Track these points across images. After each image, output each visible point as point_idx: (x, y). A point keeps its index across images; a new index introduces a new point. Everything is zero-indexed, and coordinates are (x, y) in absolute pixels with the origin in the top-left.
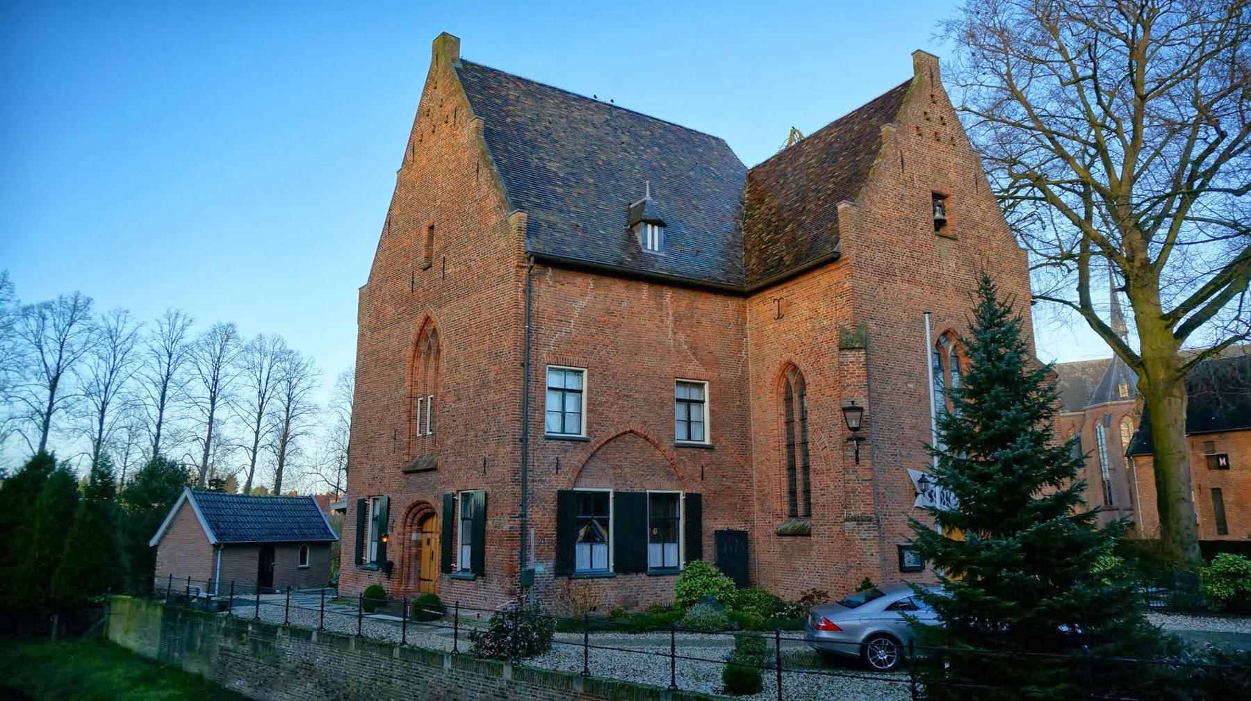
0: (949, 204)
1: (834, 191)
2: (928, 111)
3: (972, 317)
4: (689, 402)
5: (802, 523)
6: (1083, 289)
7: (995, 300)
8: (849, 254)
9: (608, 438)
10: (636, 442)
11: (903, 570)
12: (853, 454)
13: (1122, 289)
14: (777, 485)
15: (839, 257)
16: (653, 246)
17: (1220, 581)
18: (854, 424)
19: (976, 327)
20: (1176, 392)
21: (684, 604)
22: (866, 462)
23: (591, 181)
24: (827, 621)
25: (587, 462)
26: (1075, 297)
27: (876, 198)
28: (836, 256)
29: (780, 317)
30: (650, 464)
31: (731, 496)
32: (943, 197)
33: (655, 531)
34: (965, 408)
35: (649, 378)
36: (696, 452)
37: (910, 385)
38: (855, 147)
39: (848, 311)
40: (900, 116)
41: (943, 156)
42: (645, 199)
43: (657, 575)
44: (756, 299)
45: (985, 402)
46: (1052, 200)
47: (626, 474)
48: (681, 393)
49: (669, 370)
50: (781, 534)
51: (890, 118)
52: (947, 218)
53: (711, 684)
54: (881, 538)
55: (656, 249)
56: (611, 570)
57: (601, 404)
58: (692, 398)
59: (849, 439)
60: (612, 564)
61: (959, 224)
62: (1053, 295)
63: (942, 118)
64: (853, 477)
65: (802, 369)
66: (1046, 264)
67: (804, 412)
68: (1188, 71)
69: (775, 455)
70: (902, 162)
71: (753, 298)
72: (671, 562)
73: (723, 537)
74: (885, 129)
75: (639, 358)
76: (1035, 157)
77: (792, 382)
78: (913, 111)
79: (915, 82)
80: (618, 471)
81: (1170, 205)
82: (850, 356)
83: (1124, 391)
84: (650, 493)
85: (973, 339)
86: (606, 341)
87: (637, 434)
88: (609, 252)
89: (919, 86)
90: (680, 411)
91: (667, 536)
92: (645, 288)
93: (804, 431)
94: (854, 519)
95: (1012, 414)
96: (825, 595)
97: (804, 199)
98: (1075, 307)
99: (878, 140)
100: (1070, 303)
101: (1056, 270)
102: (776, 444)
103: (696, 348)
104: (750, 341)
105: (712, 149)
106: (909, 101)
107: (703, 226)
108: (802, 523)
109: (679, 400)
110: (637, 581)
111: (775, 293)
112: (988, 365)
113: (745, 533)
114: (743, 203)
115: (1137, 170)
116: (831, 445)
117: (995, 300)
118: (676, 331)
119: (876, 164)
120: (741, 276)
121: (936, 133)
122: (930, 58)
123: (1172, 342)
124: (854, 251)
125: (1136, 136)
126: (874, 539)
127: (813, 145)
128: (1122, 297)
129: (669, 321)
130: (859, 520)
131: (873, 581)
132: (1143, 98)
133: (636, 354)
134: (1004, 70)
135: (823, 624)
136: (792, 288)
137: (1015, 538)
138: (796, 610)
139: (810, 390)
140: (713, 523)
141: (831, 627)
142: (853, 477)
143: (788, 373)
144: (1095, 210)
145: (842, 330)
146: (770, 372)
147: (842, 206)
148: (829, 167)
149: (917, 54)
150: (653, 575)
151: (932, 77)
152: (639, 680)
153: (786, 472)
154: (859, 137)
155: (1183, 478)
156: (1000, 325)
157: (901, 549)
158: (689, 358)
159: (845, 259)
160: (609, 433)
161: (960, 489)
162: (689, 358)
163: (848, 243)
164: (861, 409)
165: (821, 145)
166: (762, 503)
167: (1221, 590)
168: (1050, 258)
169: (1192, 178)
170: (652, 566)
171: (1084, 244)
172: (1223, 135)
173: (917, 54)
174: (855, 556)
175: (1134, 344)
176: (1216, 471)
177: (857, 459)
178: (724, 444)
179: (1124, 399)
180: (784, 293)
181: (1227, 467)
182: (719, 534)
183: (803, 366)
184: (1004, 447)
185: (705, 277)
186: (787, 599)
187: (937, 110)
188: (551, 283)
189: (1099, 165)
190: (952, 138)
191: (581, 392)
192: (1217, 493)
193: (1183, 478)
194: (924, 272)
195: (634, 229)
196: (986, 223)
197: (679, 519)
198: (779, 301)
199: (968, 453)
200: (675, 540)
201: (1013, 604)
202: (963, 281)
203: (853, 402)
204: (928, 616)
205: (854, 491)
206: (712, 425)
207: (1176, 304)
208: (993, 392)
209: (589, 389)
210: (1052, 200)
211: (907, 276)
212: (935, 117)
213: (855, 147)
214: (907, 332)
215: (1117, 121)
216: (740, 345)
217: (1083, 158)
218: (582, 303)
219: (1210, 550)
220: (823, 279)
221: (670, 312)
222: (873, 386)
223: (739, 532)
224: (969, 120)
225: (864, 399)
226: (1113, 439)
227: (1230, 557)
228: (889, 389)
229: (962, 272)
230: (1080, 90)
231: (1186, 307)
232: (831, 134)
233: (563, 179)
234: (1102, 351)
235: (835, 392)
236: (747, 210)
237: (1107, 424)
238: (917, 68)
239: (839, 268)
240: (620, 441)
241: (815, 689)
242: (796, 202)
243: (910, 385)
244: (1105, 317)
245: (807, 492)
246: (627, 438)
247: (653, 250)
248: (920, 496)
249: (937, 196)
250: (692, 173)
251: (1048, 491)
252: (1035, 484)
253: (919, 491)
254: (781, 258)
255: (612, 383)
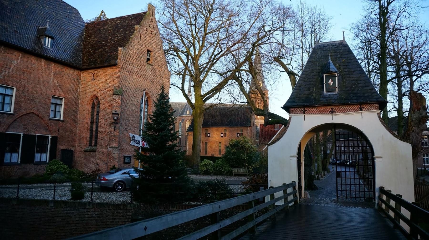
0: (152, 54)
1: (117, 42)
2: (150, 24)
3: (158, 97)
4: (56, 104)
5: (93, 148)
6: (183, 84)
7: (164, 92)
8: (120, 64)
9: (23, 114)
10: (33, 117)
11: (125, 163)
12: (114, 127)
13: (192, 86)
14: (86, 135)
15: (117, 65)
16: (48, 45)
17: (203, 166)
18: (115, 118)
19: (159, 99)
20: (201, 116)
21: (49, 174)
22: (118, 130)
23: (23, 13)
24: (104, 178)
25: (13, 122)
26: (180, 86)
27: (131, 48)
28: (116, 64)
29: (93, 80)
30: (39, 125)
31: (68, 138)
32: (151, 52)
33: (38, 149)
34: (153, 120)
35: (41, 94)
36: (56, 122)
37: (133, 108)
38: (126, 28)
39: (117, 82)
40: (142, 23)
41: (152, 39)
42: (46, 27)
43: (37, 164)
44: (85, 72)
45: (159, 120)
46: (179, 56)
47: (29, 128)
48: (53, 101)
49: (50, 92)
50: (85, 151)
51: (138, 23)
52: (150, 58)
53: (66, 198)
54: (119, 153)
55: (49, 47)
56: (19, 162)
57: (21, 102)
58: (57, 103)
59: (113, 123)
60: (19, 160)
61: (154, 61)
62: (175, 84)
63: (154, 27)
64: (112, 135)
65: (99, 98)
66: (174, 74)
67: (98, 112)
68: (218, 29)
69: (86, 125)
70: (140, 38)
71: (84, 71)
72: (44, 159)
73: (64, 151)
74: (136, 26)
75: (38, 86)
76: (177, 41)
77: (95, 102)
78: (146, 22)
79: (148, 13)
80: (25, 126)
81: (207, 65)
82: (117, 97)
83: (188, 113)
84: (38, 135)
85: (157, 102)
86: (25, 78)
87: (35, 114)
88: (28, 44)
89: (148, 15)
90: (52, 107)
91: (43, 150)
92: (43, 62)
93: (98, 118)
94: (112, 147)
95: (165, 123)
96: (100, 170)
97: (106, 41)
98: (180, 89)
99: (134, 29)
100: (179, 88)
101: (177, 76)
102: (87, 122)
103: (61, 86)
104: (81, 85)
105: (73, 12)
106: (145, 19)
107: (68, 41)
108: (93, 148)
109: (53, 103)
110: (29, 167)
111: (93, 71)
112: (160, 110)
113: (72, 151)
114: (83, 36)
115: (202, 52)
116: (106, 124)
117: (164, 92)
118: (54, 78)
119: (132, 37)
120: (80, 63)
121: (151, 31)
122: (153, 7)
123: (202, 103)
124: (122, 64)
125: (203, 44)
126: (117, 154)
127: (111, 23)
128: (192, 89)
129: (52, 75)
130: (113, 148)
131: (116, 166)
132: (206, 34)
133: (37, 85)
134: (172, 13)
135: (103, 179)
136: (99, 71)
137: (162, 155)
138: (90, 175)
139: (101, 105)
140: (62, 147)
141: (105, 180)
142: (112, 135)
143: (94, 99)
144: (189, 61)
145: (115, 88)
146: (88, 98)
147: (120, 48)
148: (116, 32)
149: (150, 4)
150: (36, 164)
151: (153, 13)
152: (39, 198)
153: (89, 131)
154: (127, 25)
155: (199, 139)
156: (165, 99)
157: (125, 157)
158: (58, 89)
159: (119, 66)
160: (23, 112)
161: (149, 142)
162: (58, 89)
163: (120, 61)
164: (118, 114)
165: (114, 24)
166: (79, 141)
167: (203, 169)
168: (176, 73)
169: (214, 59)
170: (36, 161)
171: (185, 70)
172: (222, 51)
173: (150, 4)
174: (110, 159)
175: (193, 101)
176: (207, 138)
177: (115, 129)
178: (68, 120)
179: (188, 115)
180: (96, 72)
181: (209, 137)
182: (63, 150)
183: (100, 97)
184: (162, 132)
185: (68, 61)
186: (86, 172)
187: (153, 24)
188: (3, 52)
189: (192, 48)
190: (156, 34)
191: (12, 96)
192: (206, 143)
193: (199, 139)
194: (142, 74)
195: (41, 37)
196: (161, 62)
197: (48, 145)
198: (94, 74)
199: (152, 133)
200: (46, 152)
201: (159, 171)
202: (152, 78)
203: (116, 112)
204: (136, 176)
205: (113, 139)
206: (64, 113)
207: (205, 93)
208: (161, 117)
209: (16, 95)
210: (179, 56)
211: (137, 74)
212: (152, 26)
213: (126, 28)
214: (135, 91)
215: (199, 38)
216: (78, 87)
217: (189, 45)
218: (16, 62)
219: (203, 158)
220: (110, 71)
221: (53, 71)
222: (122, 107)
223: (70, 150)
224: (160, 26)
225: (119, 111)
226: (184, 126)
227: (206, 160)
228: (127, 108)
229: (152, 76)
230: (191, 26)
231: (207, 94)
232: (118, 21)
233: (10, 10)
234: (185, 101)
235: (109, 107)
236: (85, 39)
237: (182, 122)
238: (149, 9)
239: (116, 68)
240: (28, 116)
241: (100, 197)
242: (103, 41)
243: (133, 108)
244: (187, 93)
245: (96, 138)
246: (30, 115)
247: (48, 47)
248: (132, 142)
249: (149, 51)
250: (64, 20)
251: (170, 143)
252: (167, 141)
253: (132, 140)
254: (96, 60)
255: (26, 94)
